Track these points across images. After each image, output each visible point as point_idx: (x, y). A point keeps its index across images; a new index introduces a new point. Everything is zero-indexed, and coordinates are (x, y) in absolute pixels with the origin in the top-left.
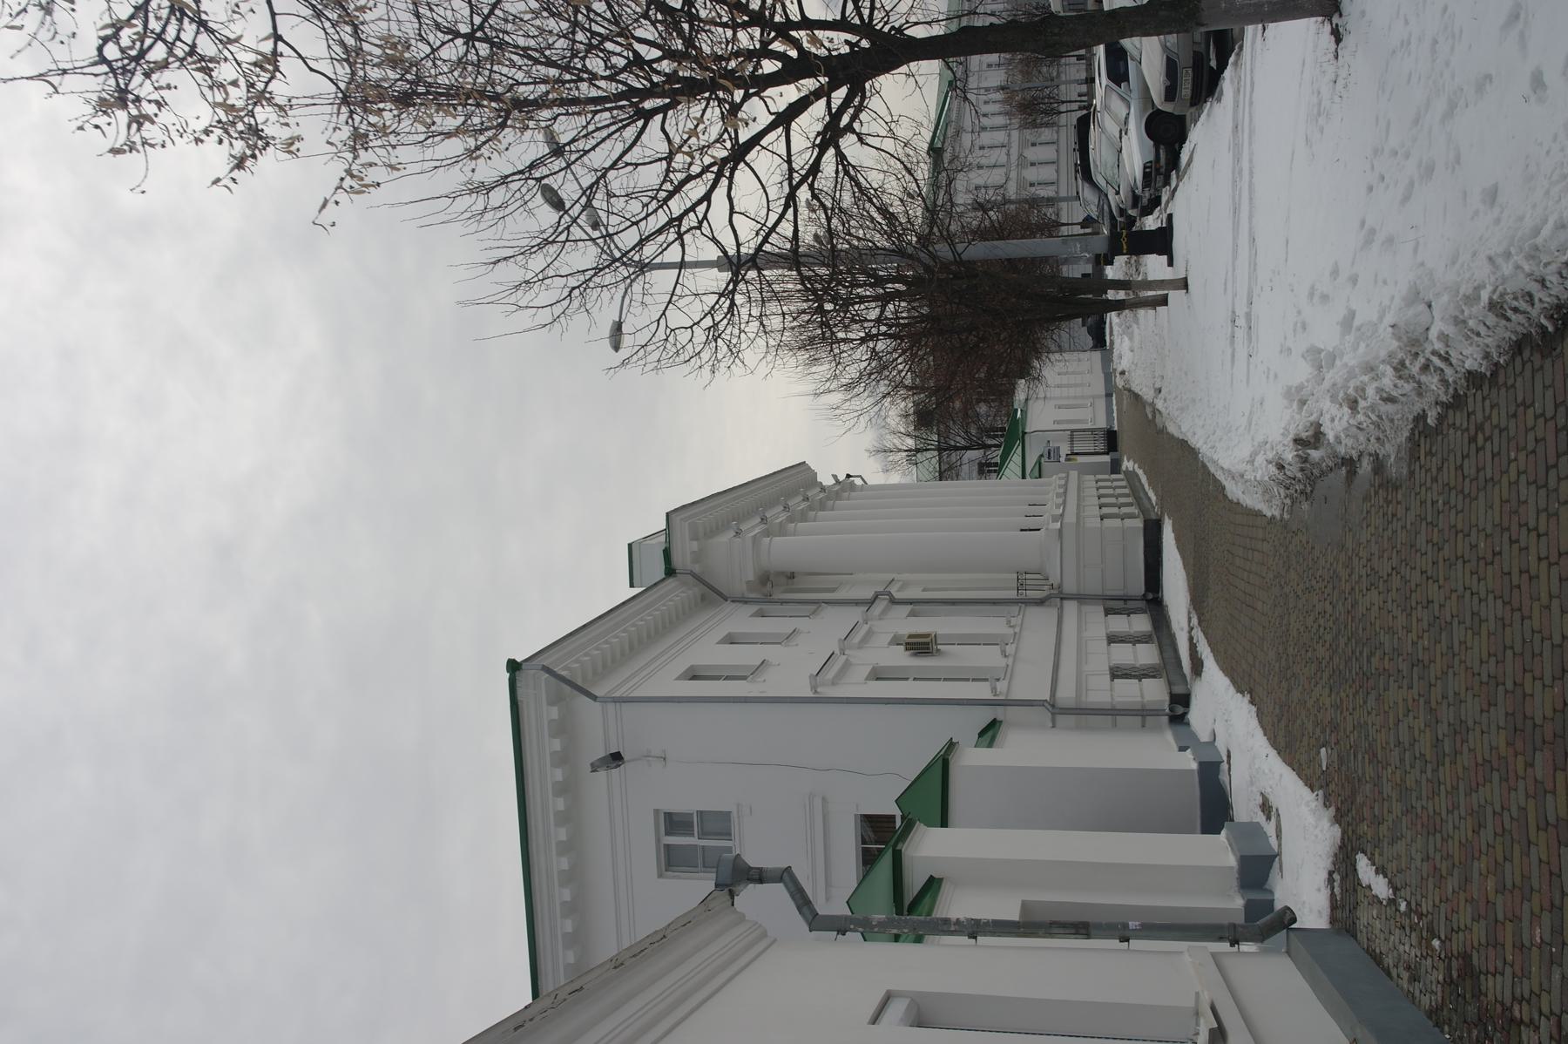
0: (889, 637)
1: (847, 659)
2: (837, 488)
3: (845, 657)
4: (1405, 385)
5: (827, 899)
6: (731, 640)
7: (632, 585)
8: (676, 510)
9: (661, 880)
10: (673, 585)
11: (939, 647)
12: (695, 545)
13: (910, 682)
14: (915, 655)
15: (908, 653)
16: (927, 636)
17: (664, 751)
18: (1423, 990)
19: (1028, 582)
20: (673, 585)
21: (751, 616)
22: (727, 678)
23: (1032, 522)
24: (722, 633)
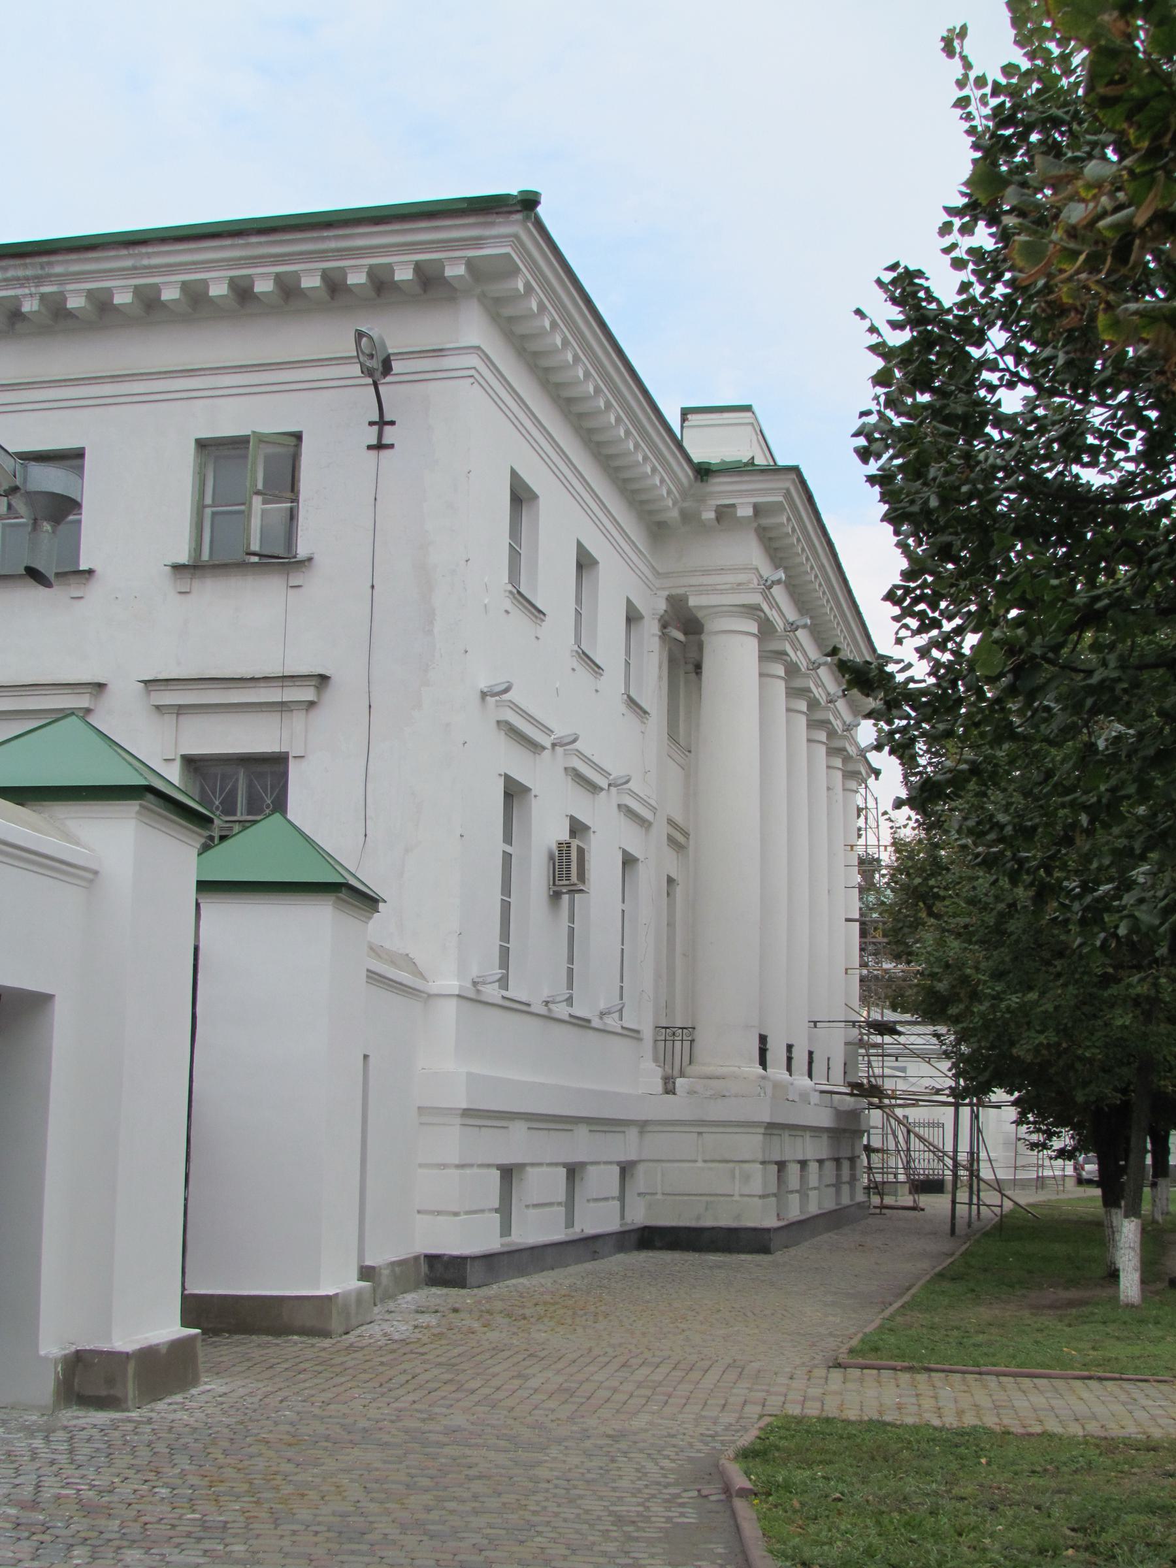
0: (674, 875)
1: (602, 789)
2: (852, 750)
3: (606, 787)
4: (1087, 1478)
5: (158, 707)
6: (585, 563)
7: (685, 413)
8: (803, 483)
9: (193, 444)
10: (684, 481)
11: (566, 897)
12: (745, 511)
13: (502, 847)
14: (551, 857)
15: (554, 847)
16: (582, 876)
17: (391, 446)
18: (358, 1505)
19: (678, 1044)
20: (684, 481)
21: (629, 601)
22: (578, 613)
23: (777, 1053)
24: (597, 547)
